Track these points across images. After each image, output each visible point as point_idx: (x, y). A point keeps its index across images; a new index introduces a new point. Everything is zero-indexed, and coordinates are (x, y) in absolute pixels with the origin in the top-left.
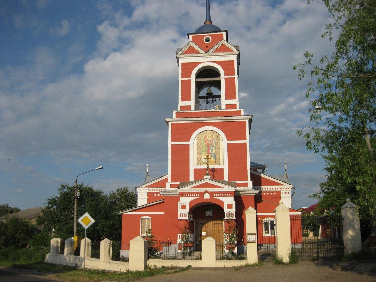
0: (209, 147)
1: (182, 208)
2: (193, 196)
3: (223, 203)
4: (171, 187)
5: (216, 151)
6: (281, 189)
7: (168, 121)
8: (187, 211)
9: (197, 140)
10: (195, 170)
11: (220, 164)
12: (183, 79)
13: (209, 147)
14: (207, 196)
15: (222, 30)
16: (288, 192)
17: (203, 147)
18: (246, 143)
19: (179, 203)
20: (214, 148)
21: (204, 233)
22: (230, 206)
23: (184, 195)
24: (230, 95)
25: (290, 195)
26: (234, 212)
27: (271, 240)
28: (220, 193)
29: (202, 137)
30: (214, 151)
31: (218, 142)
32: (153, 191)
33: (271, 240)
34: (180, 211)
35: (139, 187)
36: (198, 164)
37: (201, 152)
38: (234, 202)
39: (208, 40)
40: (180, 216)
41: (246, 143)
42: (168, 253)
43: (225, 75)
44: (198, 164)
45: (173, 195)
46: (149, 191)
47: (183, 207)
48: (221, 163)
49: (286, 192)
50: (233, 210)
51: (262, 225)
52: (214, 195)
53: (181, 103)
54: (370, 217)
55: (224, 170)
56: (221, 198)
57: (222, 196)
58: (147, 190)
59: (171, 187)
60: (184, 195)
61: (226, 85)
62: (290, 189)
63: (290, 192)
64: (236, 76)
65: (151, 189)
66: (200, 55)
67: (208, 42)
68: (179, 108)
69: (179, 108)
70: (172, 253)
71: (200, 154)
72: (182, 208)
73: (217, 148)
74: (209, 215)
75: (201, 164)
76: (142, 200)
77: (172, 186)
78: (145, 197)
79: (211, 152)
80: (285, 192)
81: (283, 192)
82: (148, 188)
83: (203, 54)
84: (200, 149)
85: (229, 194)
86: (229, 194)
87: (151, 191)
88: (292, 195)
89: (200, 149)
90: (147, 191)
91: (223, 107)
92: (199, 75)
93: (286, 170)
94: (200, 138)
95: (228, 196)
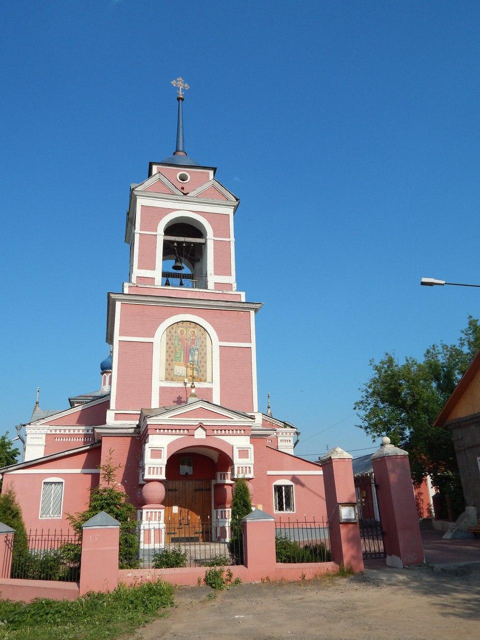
0: (188, 352)
1: (152, 456)
4: (116, 419)
5: (200, 356)
8: (163, 461)
9: (167, 335)
10: (162, 389)
11: (205, 381)
12: (141, 232)
13: (188, 352)
14: (200, 434)
16: (288, 439)
17: (177, 349)
19: (147, 445)
20: (197, 352)
21: (175, 509)
22: (244, 453)
24: (222, 269)
25: (292, 444)
26: (251, 464)
27: (156, 516)
29: (176, 332)
30: (196, 358)
32: (58, 432)
33: (156, 516)
36: (167, 379)
38: (252, 446)
40: (149, 473)
43: (215, 236)
44: (167, 379)
45: (11, 467)
47: (156, 453)
48: (209, 379)
50: (250, 461)
51: (371, 486)
53: (137, 272)
58: (47, 429)
59: (116, 419)
61: (215, 256)
62: (292, 434)
63: (292, 439)
67: (184, 182)
68: (134, 280)
71: (172, 360)
72: (152, 456)
74: (187, 474)
75: (172, 380)
76: (34, 450)
78: (41, 443)
79: (190, 359)
80: (284, 438)
81: (282, 438)
82: (48, 426)
87: (53, 432)
88: (295, 444)
89: (172, 352)
91: (211, 285)
93: (269, 407)
94: (173, 331)
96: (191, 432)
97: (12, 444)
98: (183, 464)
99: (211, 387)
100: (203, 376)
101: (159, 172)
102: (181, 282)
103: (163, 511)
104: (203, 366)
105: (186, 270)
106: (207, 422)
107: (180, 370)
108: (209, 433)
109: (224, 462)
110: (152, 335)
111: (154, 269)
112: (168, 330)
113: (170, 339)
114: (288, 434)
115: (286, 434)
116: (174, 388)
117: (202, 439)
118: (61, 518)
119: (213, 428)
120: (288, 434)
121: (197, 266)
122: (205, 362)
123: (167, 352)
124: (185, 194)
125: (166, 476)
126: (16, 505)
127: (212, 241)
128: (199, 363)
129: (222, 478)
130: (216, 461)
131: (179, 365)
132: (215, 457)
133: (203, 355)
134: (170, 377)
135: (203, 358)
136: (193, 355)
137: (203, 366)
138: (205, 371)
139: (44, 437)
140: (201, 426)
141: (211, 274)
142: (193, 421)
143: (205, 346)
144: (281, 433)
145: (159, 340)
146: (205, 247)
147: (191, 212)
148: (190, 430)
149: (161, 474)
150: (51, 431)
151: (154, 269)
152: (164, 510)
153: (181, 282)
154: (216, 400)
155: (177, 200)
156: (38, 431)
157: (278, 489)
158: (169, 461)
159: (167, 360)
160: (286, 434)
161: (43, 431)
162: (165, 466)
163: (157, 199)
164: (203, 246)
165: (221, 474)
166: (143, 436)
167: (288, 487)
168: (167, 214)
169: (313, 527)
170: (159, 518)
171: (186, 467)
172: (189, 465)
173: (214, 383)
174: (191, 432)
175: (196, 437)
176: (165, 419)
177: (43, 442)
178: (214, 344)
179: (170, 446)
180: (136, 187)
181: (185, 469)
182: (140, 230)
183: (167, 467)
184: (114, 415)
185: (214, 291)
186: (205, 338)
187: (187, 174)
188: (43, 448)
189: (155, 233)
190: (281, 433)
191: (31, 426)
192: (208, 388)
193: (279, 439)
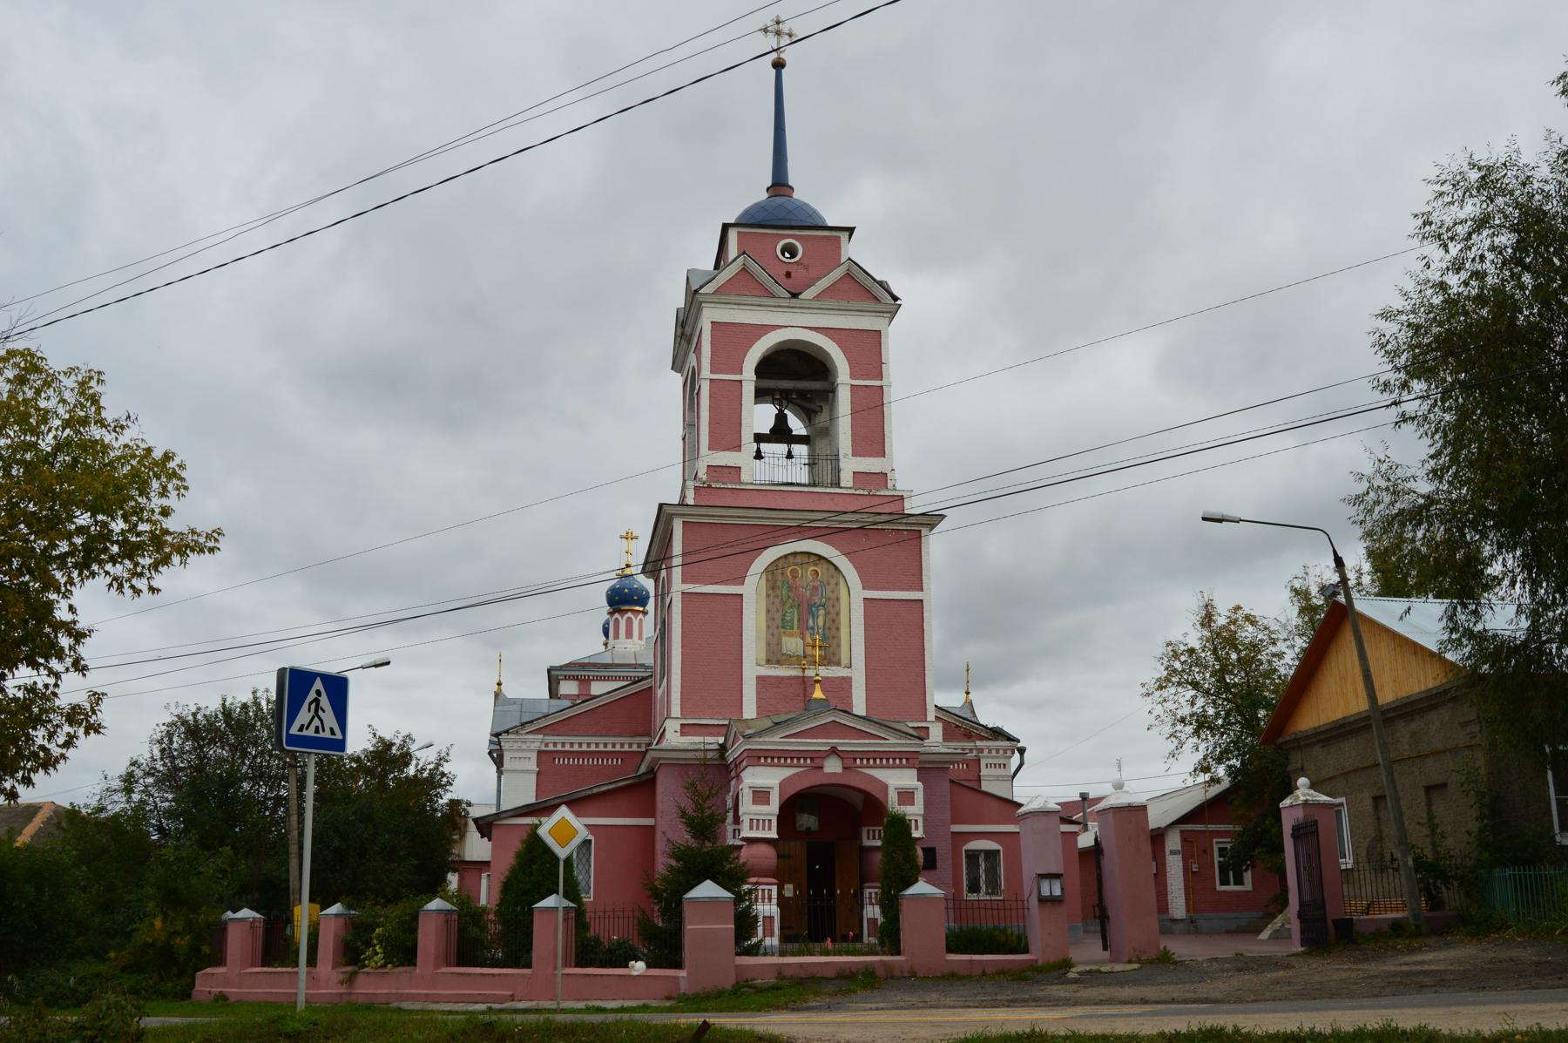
1: (755, 802)
3: (885, 787)
4: (683, 734)
6: (981, 750)
8: (774, 807)
10: (760, 679)
11: (839, 664)
14: (833, 766)
15: (830, 224)
18: (683, 582)
20: (822, 612)
22: (906, 796)
28: (875, 755)
30: (821, 621)
32: (559, 748)
34: (747, 807)
35: (507, 732)
36: (768, 661)
39: (790, 250)
41: (683, 582)
43: (853, 376)
44: (768, 661)
47: (761, 796)
48: (844, 661)
54: (173, 969)
56: (880, 774)
58: (537, 742)
59: (683, 734)
69: (702, 475)
72: (755, 802)
75: (778, 662)
77: (685, 729)
79: (811, 623)
87: (551, 748)
90: (537, 745)
91: (847, 479)
92: (763, 369)
95: (901, 767)
97: (95, 728)
98: (802, 811)
102: (789, 451)
103: (775, 889)
105: (796, 425)
106: (844, 744)
107: (793, 644)
108: (849, 763)
110: (740, 580)
113: (772, 587)
117: (835, 774)
119: (854, 756)
121: (822, 419)
122: (838, 629)
124: (795, 295)
126: (1202, 724)
130: (860, 808)
131: (791, 635)
132: (858, 801)
133: (833, 616)
134: (775, 656)
136: (815, 617)
138: (839, 646)
139: (534, 756)
142: (820, 744)
145: (752, 590)
148: (816, 758)
153: (789, 451)
154: (859, 707)
157: (973, 856)
161: (533, 746)
167: (991, 855)
168: (760, 337)
170: (770, 899)
171: (806, 816)
173: (855, 669)
175: (827, 770)
177: (533, 765)
178: (854, 594)
179: (781, 785)
181: (808, 821)
182: (712, 372)
183: (779, 817)
189: (737, 377)
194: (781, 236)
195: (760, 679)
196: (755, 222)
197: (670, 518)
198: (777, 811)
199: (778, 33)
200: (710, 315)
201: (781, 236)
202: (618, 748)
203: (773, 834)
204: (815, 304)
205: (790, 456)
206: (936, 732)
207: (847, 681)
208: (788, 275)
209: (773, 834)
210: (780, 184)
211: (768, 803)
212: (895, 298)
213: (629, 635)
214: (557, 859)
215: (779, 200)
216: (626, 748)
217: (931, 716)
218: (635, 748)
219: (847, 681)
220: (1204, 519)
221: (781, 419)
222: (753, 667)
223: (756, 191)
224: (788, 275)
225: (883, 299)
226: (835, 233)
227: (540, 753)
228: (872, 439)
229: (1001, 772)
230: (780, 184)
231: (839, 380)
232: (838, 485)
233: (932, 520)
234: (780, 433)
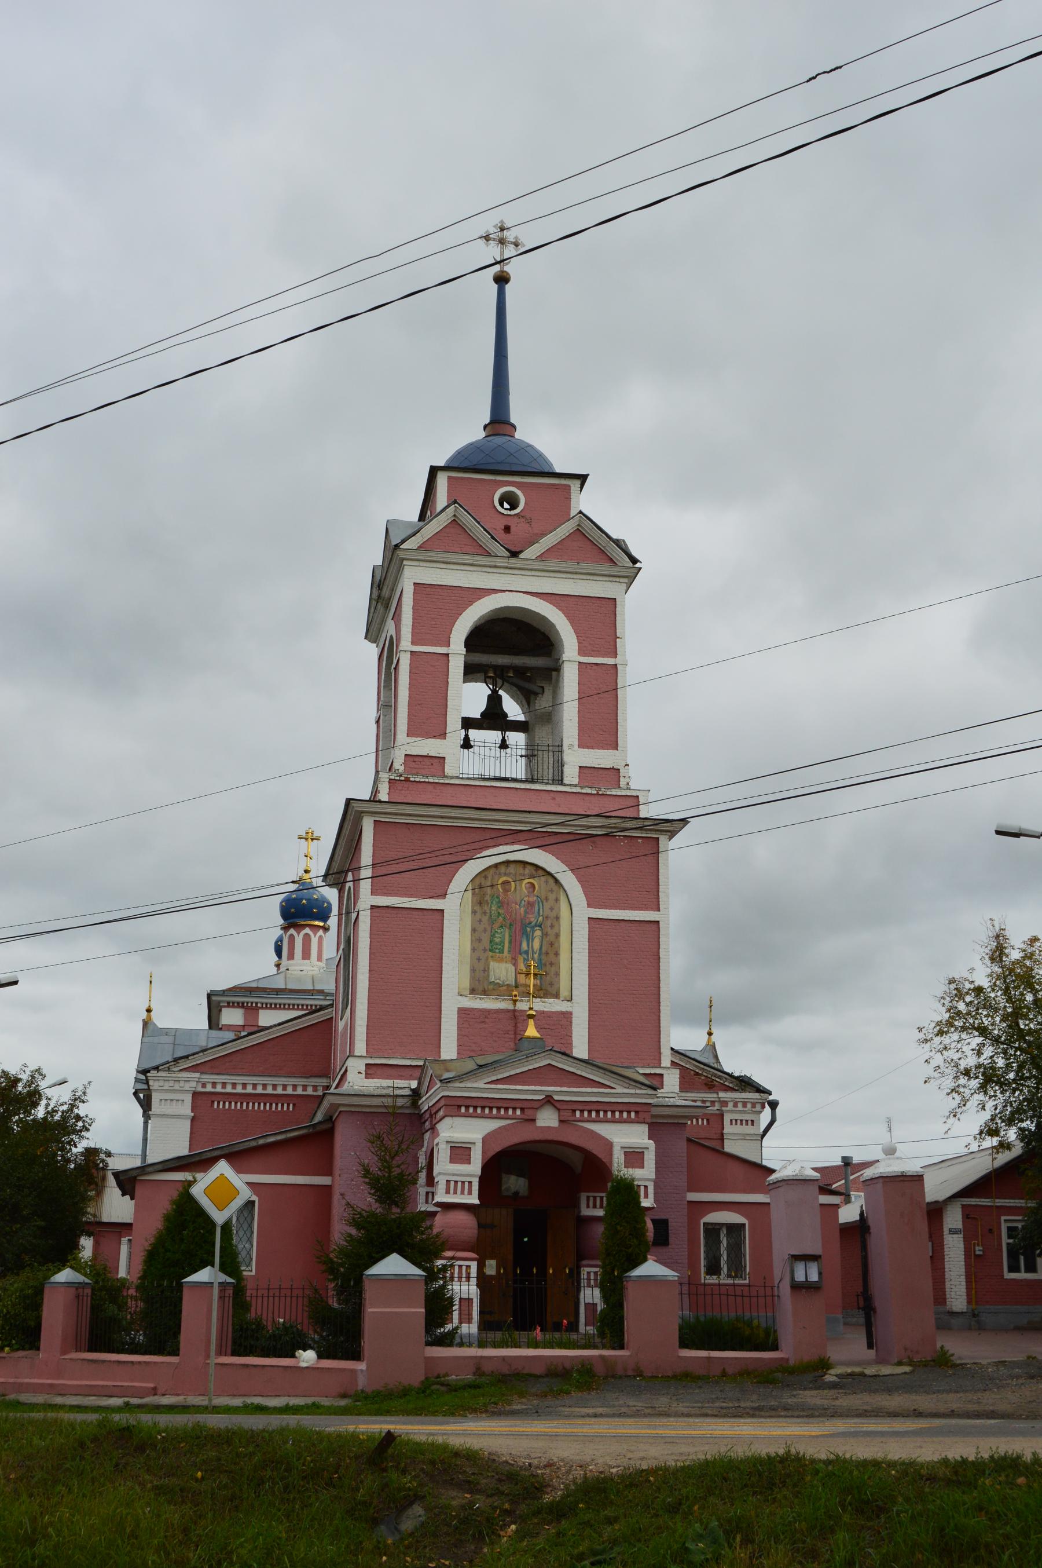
1: (453, 1160)
2: (498, 1117)
3: (609, 1145)
6: (725, 1103)
7: (363, 812)
8: (475, 1167)
10: (463, 1012)
11: (557, 996)
14: (547, 1119)
20: (538, 933)
22: (634, 1157)
23: (463, 1110)
27: (460, 1272)
30: (536, 944)
31: (552, 909)
32: (219, 1089)
33: (460, 1272)
34: (443, 1166)
35: (157, 1068)
36: (473, 991)
37: (486, 943)
39: (511, 500)
40: (448, 1192)
42: (733, 1315)
43: (582, 652)
44: (473, 991)
46: (200, 1089)
47: (460, 1153)
48: (564, 992)
49: (745, 1117)
52: (578, 1113)
55: (574, 1020)
57: (606, 1121)
58: (192, 1081)
60: (463, 1110)
64: (406, 643)
65: (208, 1078)
66: (615, 571)
70: (725, 1314)
72: (453, 1160)
73: (547, 935)
75: (485, 993)
77: (371, 1070)
79: (524, 946)
82: (197, 1075)
83: (498, 560)
84: (485, 930)
85: (633, 1115)
86: (633, 1115)
87: (209, 1088)
91: (571, 775)
92: (476, 640)
96: (529, 1113)
99: (569, 1009)
100: (551, 984)
101: (455, 502)
102: (504, 740)
104: (551, 964)
105: (513, 709)
106: (562, 1092)
107: (502, 971)
108: (567, 1115)
109: (590, 1169)
111: (443, 735)
112: (477, 882)
114: (749, 1106)
115: (745, 1105)
116: (489, 1011)
118: (253, 1273)
120: (749, 1106)
121: (543, 703)
122: (557, 954)
123: (474, 930)
124: (514, 554)
125: (481, 1197)
127: (576, 666)
128: (543, 957)
129: (452, 1191)
131: (501, 960)
132: (576, 1161)
133: (552, 938)
134: (480, 986)
135: (552, 944)
136: (530, 940)
137: (551, 964)
138: (557, 974)
139: (188, 1098)
140: (549, 1101)
141: (571, 746)
143: (558, 918)
144: (731, 1105)
145: (455, 905)
146: (559, 675)
147: (529, 596)
148: (528, 1109)
149: (470, 1193)
150: (204, 1085)
151: (443, 735)
152: (475, 1263)
153: (504, 740)
155: (495, 567)
156: (177, 1087)
157: (713, 1231)
158: (484, 1168)
159: (473, 950)
160: (745, 1105)
162: (478, 1179)
163: (449, 566)
164: (554, 673)
165: (588, 1198)
166: (427, 1115)
167: (735, 1229)
168: (471, 603)
169: (746, 1293)
170: (468, 1278)
171: (513, 1178)
172: (520, 1175)
174: (529, 1113)
175: (540, 1123)
176: (478, 1087)
177: (186, 1109)
178: (577, 913)
179: (485, 1140)
180: (403, 541)
181: (515, 1183)
182: (413, 643)
183: (482, 1180)
184: (363, 1069)
185: (578, 790)
186: (557, 900)
187: (519, 493)
188: (188, 1123)
189: (610, 661)
190: (731, 1105)
191: (161, 1074)
192: (562, 1013)
193: (727, 1119)
194: (499, 484)
195: (463, 1012)
196: (469, 465)
197: (359, 816)
198: (478, 1171)
199: (502, 242)
200: (412, 575)
201: (499, 484)
202: (290, 1091)
203: (474, 1200)
204: (539, 565)
205: (504, 745)
206: (672, 1081)
207: (567, 1016)
208: (507, 529)
209: (474, 1200)
210: (499, 421)
211: (468, 1161)
212: (634, 561)
213: (306, 955)
214: (212, 1224)
215: (498, 440)
216: (300, 1091)
217: (666, 1062)
218: (310, 1091)
219: (567, 1016)
220: (998, 833)
221: (494, 701)
222: (454, 998)
223: (471, 430)
224: (507, 529)
225: (615, 558)
226: (563, 482)
227: (195, 1094)
228: (603, 726)
229: (748, 1129)
230: (499, 421)
231: (565, 656)
232: (561, 782)
233: (672, 826)
234: (493, 717)
